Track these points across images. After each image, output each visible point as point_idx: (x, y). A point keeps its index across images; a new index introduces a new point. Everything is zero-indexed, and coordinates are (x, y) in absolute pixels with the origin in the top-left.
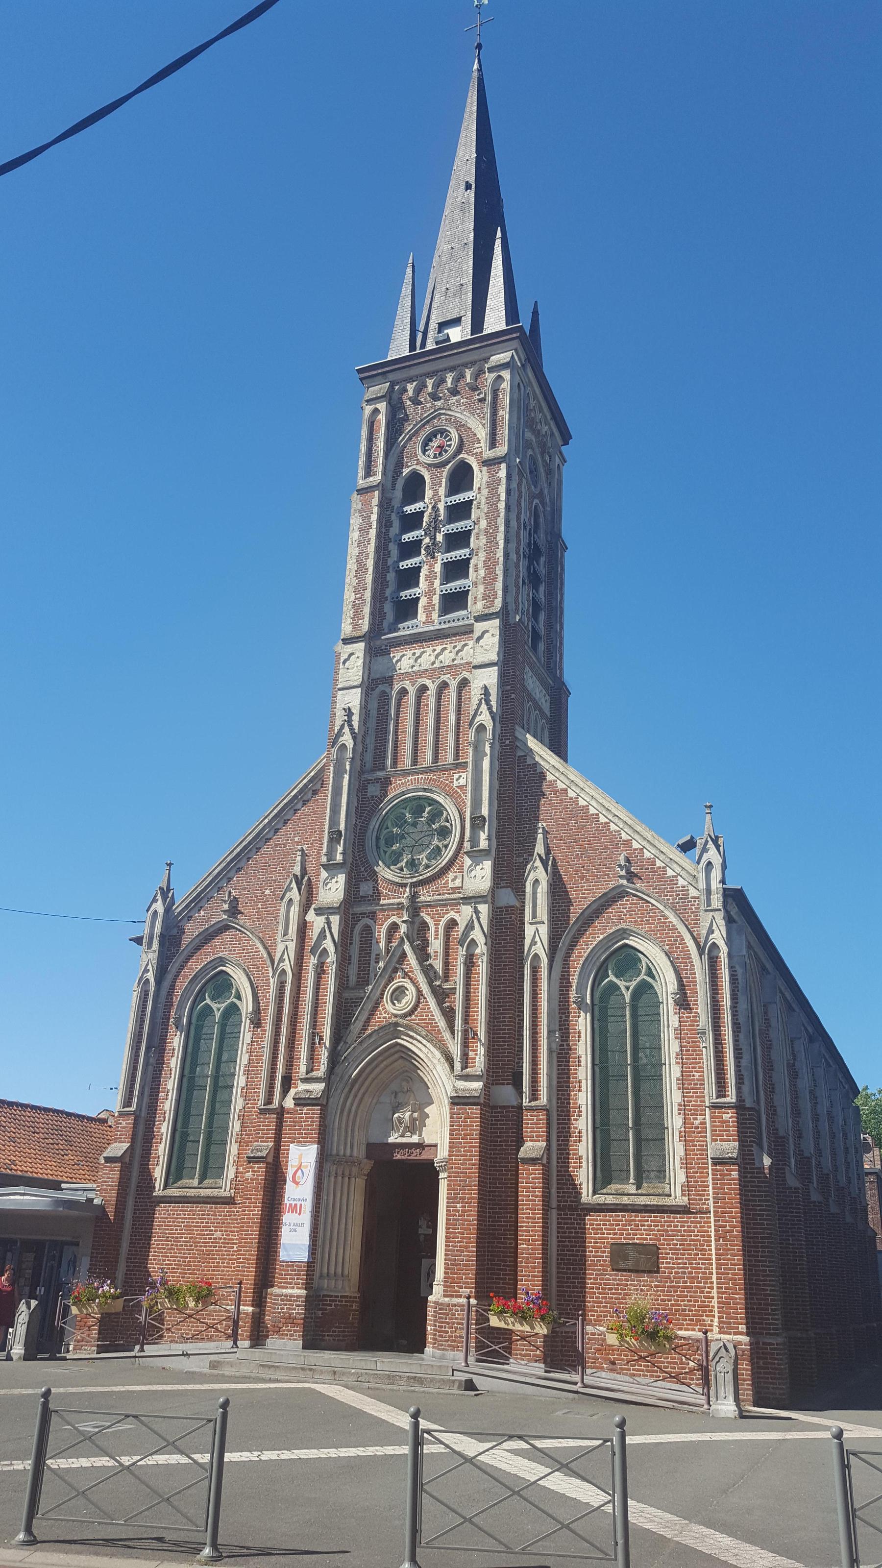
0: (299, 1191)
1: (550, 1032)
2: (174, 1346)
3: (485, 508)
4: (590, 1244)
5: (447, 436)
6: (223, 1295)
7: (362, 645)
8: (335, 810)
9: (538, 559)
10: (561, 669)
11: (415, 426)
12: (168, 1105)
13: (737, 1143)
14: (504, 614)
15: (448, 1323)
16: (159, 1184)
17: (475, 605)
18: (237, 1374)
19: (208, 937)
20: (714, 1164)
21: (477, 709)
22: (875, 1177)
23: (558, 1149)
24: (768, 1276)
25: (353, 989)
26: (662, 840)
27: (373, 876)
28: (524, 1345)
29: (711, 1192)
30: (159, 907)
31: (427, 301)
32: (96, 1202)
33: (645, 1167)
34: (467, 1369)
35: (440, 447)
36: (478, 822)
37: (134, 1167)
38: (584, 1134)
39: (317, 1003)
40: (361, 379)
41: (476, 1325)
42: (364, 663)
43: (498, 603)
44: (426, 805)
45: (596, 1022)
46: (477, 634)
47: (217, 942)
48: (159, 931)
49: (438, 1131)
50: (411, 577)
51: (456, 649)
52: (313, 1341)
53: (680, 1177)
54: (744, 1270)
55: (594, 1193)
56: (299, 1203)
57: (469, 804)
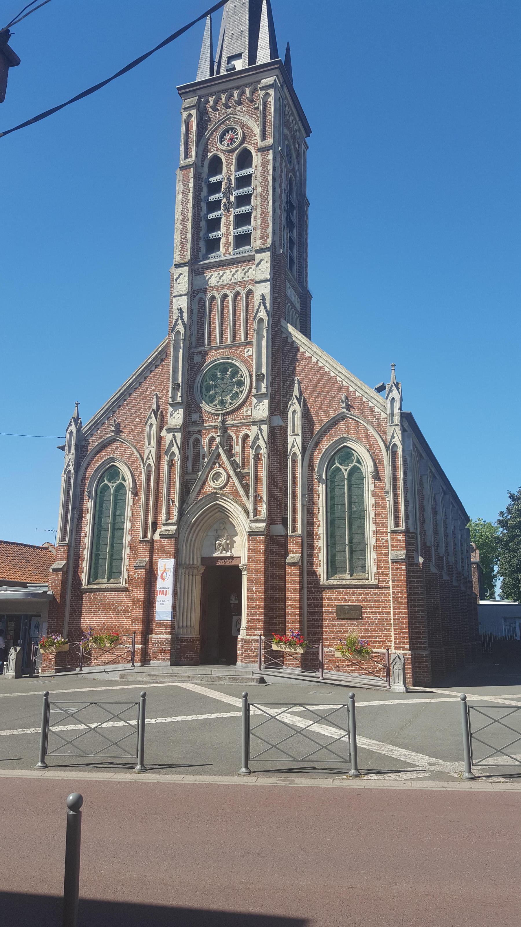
0: (165, 584)
1: (303, 495)
2: (98, 667)
3: (260, 179)
4: (325, 606)
5: (235, 132)
6: (124, 640)
7: (186, 269)
8: (175, 371)
9: (293, 211)
10: (307, 282)
11: (215, 125)
12: (87, 540)
13: (405, 551)
14: (273, 249)
15: (249, 649)
16: (84, 582)
17: (256, 243)
18: (136, 680)
19: (103, 446)
20: (393, 562)
21: (258, 309)
22: (476, 565)
23: (308, 557)
24: (421, 619)
25: (190, 474)
26: (366, 386)
27: (200, 409)
28: (290, 659)
29: (390, 577)
30: (73, 428)
31: (220, 42)
32: (48, 593)
33: (355, 565)
34: (260, 672)
35: (231, 139)
36: (260, 377)
37: (70, 573)
38: (321, 549)
39: (170, 482)
40: (180, 94)
41: (264, 649)
42: (189, 279)
43: (270, 241)
44: (229, 367)
45: (328, 489)
46: (257, 261)
47: (109, 448)
48: (74, 442)
49: (241, 549)
50: (215, 224)
51: (245, 271)
52: (176, 660)
53: (374, 569)
54: (408, 617)
55: (327, 579)
56: (165, 590)
57: (254, 367)
